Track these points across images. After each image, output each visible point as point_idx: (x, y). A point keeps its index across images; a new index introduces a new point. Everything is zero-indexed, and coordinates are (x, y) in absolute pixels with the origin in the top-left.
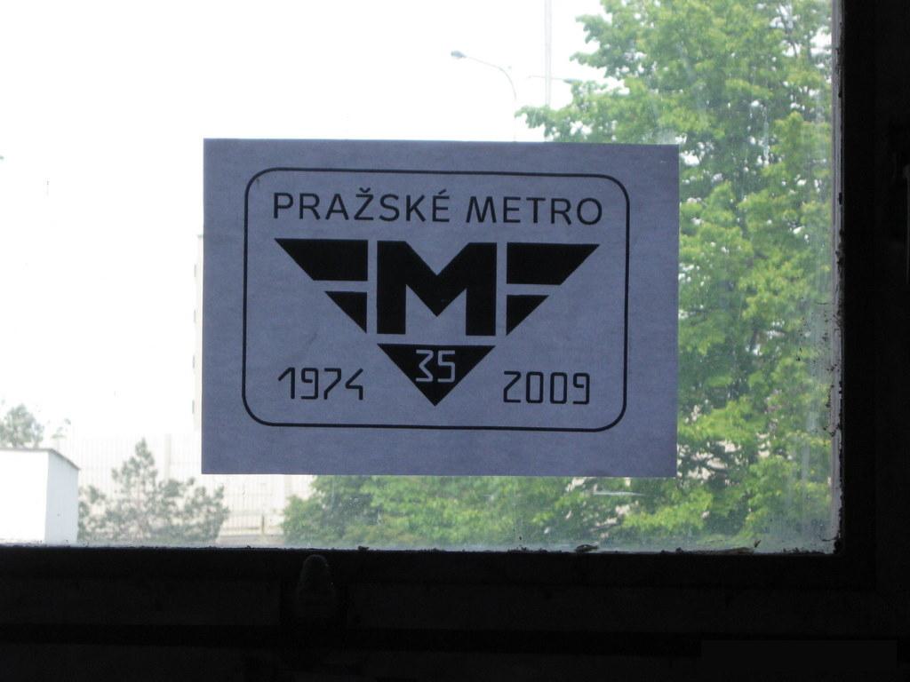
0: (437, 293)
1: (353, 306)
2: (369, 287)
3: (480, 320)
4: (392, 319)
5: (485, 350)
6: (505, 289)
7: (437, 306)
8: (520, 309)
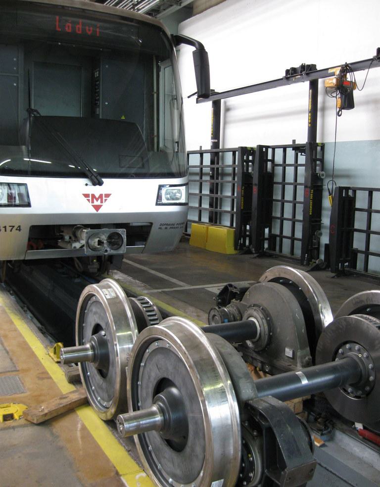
0: (97, 200)
1: (89, 200)
2: (90, 198)
3: (102, 202)
4: (93, 202)
5: (102, 205)
6: (104, 198)
7: (97, 201)
8: (106, 200)
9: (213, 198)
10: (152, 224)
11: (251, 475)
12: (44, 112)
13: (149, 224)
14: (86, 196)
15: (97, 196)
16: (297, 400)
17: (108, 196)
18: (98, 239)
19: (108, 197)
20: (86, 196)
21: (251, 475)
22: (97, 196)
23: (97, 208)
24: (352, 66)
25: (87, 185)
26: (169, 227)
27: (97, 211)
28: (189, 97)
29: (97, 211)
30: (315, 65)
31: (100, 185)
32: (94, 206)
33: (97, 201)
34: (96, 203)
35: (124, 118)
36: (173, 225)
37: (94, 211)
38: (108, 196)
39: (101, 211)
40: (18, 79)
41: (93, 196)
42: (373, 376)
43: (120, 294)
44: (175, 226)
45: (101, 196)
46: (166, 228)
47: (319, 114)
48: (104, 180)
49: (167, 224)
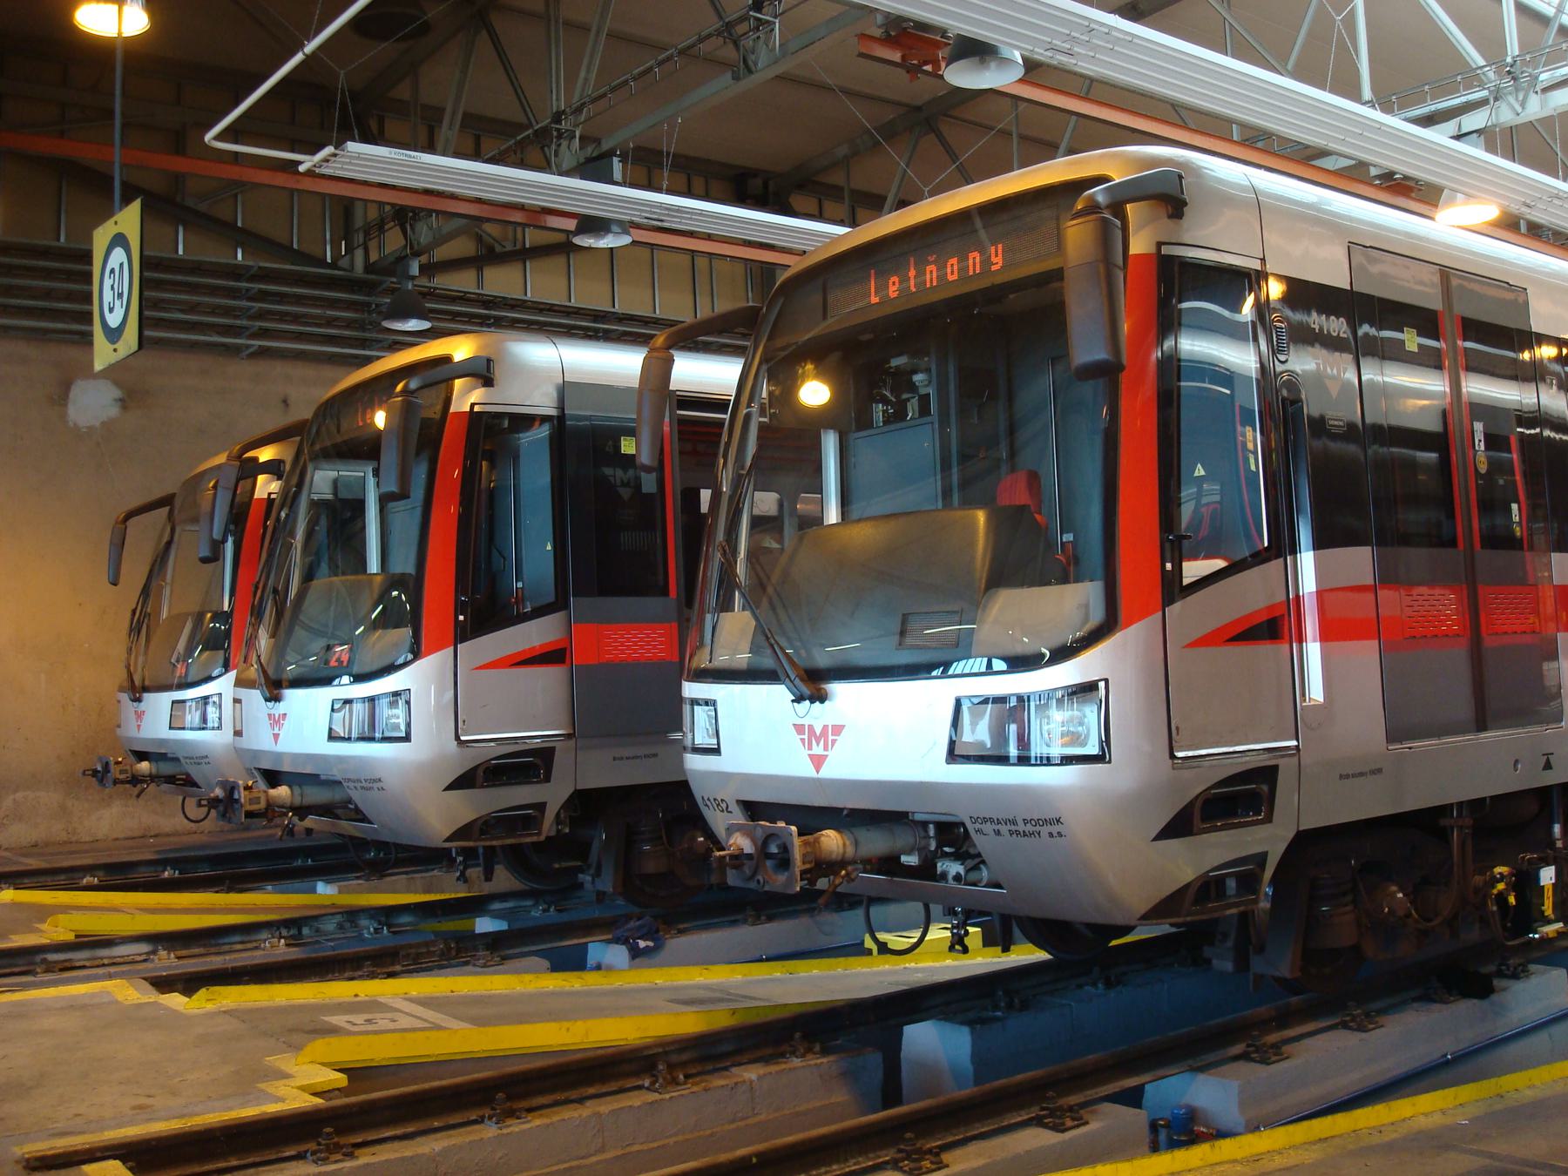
3: (826, 748)
4: (810, 748)
8: (834, 742)
12: (909, 406)
14: (799, 729)
17: (838, 730)
18: (272, 792)
20: (799, 729)
23: (818, 761)
26: (1004, 829)
31: (822, 701)
34: (818, 750)
35: (1202, 473)
37: (808, 771)
38: (838, 730)
39: (827, 772)
42: (983, 1062)
43: (211, 910)
47: (666, 225)
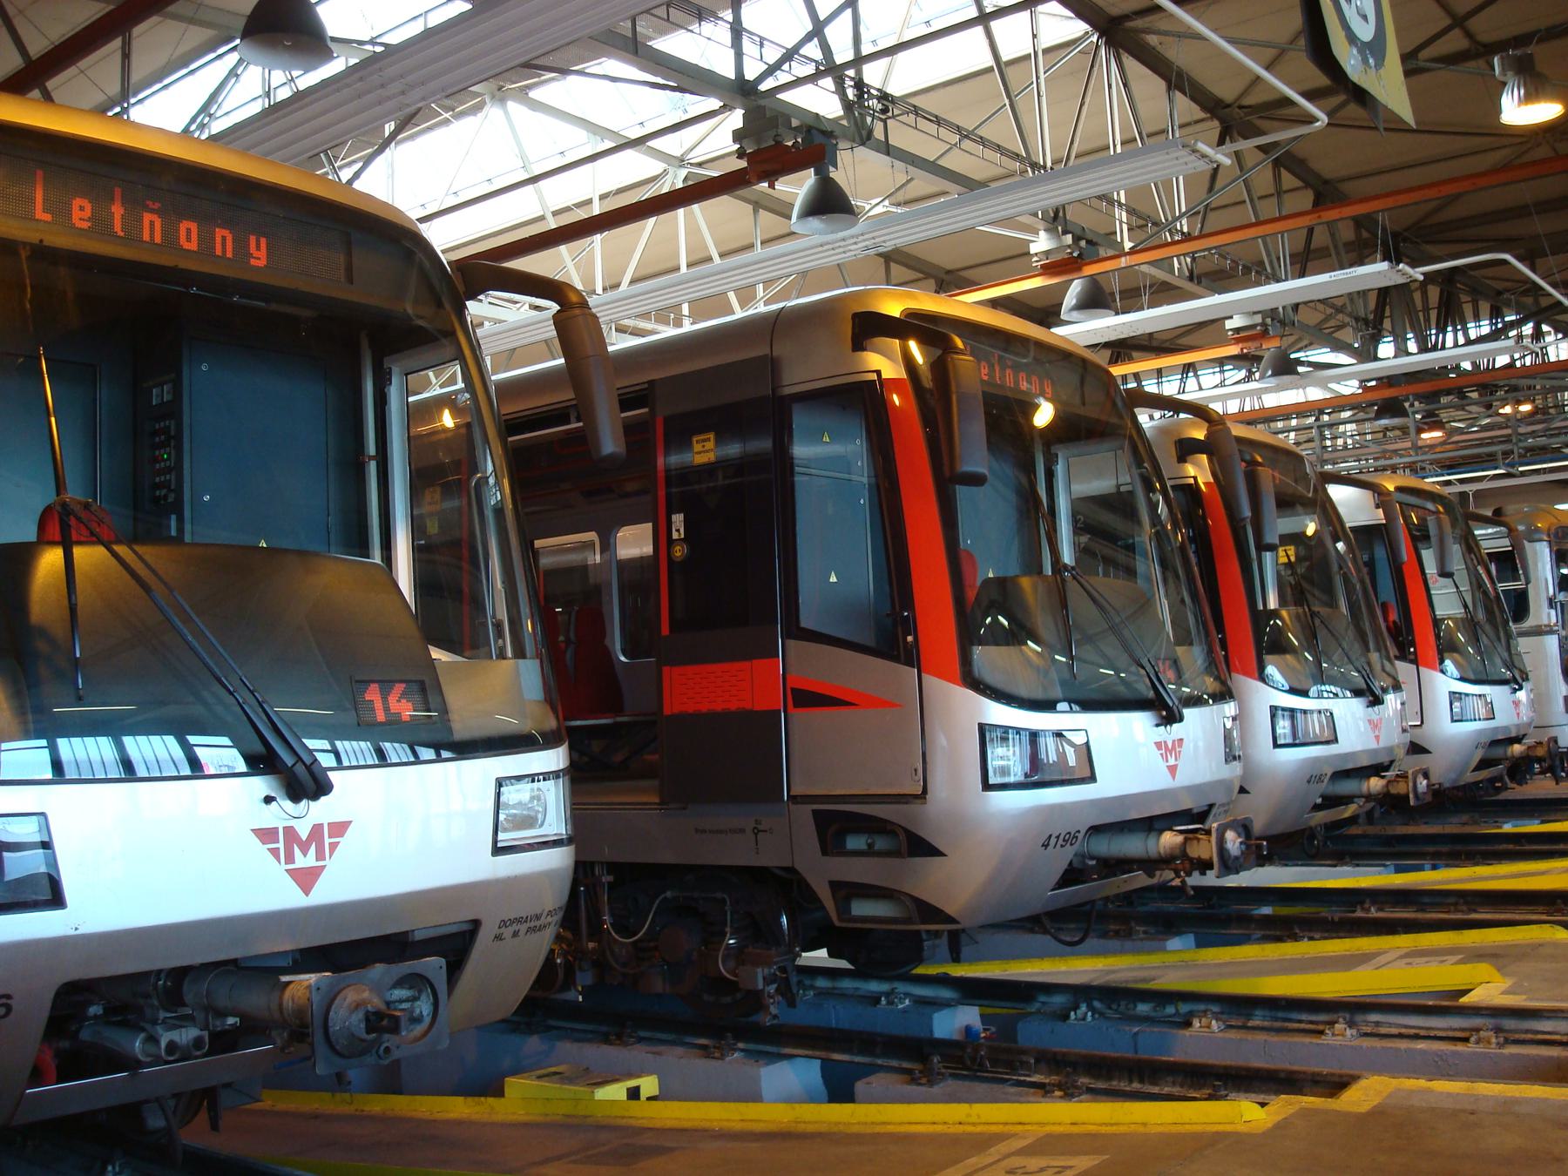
1: (275, 852)
2: (281, 845)
3: (320, 856)
4: (290, 858)
6: (327, 841)
7: (305, 853)
8: (333, 846)
9: (276, 829)
10: (476, 924)
11: (826, 439)
13: (465, 927)
14: (267, 835)
15: (304, 836)
16: (932, 970)
17: (339, 828)
19: (341, 835)
20: (267, 835)
21: (826, 439)
22: (304, 836)
23: (305, 879)
24: (965, 274)
25: (268, 800)
26: (523, 928)
27: (307, 892)
28: (350, 280)
29: (307, 892)
30: (825, 852)
32: (294, 874)
33: (305, 853)
34: (304, 861)
36: (538, 917)
38: (339, 828)
39: (326, 892)
40: (1327, 742)
41: (290, 832)
44: (543, 921)
45: (317, 830)
46: (516, 934)
48: (1186, 712)
49: (519, 920)
